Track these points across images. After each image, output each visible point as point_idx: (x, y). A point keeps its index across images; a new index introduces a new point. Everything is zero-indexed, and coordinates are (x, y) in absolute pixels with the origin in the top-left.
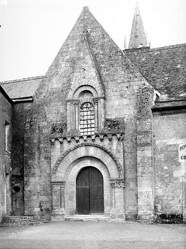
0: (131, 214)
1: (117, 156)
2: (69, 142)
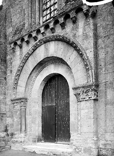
0: (108, 147)
1: (84, 47)
2: (28, 42)
